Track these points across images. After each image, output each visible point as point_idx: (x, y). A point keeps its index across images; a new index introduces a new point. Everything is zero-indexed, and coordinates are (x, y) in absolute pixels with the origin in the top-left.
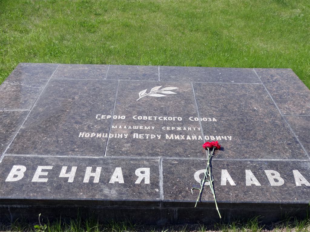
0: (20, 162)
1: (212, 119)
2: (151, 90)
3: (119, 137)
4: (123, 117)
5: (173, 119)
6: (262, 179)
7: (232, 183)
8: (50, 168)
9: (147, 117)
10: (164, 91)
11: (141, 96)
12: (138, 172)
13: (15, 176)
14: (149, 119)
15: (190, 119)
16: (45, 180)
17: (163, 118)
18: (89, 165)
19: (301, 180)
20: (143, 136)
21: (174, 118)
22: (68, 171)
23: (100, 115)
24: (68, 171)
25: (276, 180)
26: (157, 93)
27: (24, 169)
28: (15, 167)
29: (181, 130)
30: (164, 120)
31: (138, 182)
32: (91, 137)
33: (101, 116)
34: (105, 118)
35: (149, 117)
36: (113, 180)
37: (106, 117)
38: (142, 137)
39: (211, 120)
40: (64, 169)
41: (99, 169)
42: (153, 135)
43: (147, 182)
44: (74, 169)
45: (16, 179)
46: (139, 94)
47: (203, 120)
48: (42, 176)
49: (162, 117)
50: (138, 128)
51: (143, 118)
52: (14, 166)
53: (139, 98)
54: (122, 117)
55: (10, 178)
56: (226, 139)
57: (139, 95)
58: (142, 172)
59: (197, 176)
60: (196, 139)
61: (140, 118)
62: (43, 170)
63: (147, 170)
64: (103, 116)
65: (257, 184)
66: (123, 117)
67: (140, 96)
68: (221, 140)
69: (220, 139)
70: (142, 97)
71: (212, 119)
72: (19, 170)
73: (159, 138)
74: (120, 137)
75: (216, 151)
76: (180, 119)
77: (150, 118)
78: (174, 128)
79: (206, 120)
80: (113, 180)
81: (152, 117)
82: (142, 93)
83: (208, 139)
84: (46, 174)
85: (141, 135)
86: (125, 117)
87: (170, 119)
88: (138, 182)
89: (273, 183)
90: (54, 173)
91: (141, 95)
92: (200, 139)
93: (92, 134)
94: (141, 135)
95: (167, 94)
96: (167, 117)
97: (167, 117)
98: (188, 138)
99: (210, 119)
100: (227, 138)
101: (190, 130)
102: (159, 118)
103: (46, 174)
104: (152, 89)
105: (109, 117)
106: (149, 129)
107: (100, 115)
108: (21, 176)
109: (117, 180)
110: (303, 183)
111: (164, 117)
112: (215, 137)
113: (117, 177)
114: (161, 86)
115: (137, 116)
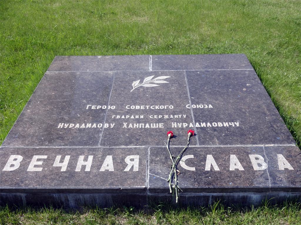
0: (17, 152)
1: (208, 106)
2: (144, 80)
3: (135, 127)
4: (113, 107)
5: (164, 108)
6: (272, 162)
7: (217, 168)
8: (45, 157)
9: (139, 106)
10: (157, 80)
11: (135, 87)
12: (127, 160)
13: (12, 166)
14: (141, 108)
15: (127, 107)
16: (40, 169)
17: (154, 107)
18: (59, 153)
19: (284, 164)
20: (162, 125)
21: (166, 106)
22: (62, 161)
23: (91, 105)
24: (62, 161)
25: (260, 165)
26: (150, 83)
27: (20, 158)
28: (13, 157)
29: (168, 117)
30: (156, 108)
31: (127, 169)
32: (70, 127)
33: (91, 107)
34: (95, 109)
35: (142, 106)
36: (102, 169)
37: (96, 107)
38: (162, 126)
39: (207, 107)
40: (59, 157)
41: (91, 158)
42: (185, 123)
43: (136, 169)
44: (67, 158)
45: (12, 169)
46: (133, 85)
47: (199, 107)
48: (229, 191)
49: (154, 106)
50: (140, 124)
51: (135, 107)
52: (128, 157)
53: (133, 88)
54: (112, 106)
55: (7, 168)
56: (233, 126)
57: (133, 86)
58: (132, 160)
59: (183, 164)
60: (205, 126)
61: (133, 107)
62: (39, 160)
63: (137, 158)
64: (93, 106)
65: (241, 169)
66: (113, 107)
67: (134, 87)
68: (234, 126)
69: (228, 126)
70: (135, 88)
71: (208, 106)
72: (15, 160)
73: (238, 126)
74: (136, 124)
75: (191, 137)
76: (171, 107)
77: (142, 107)
78: (187, 125)
79: (203, 107)
80: (102, 169)
81: (144, 106)
82: (136, 84)
83: (222, 125)
84: (40, 163)
85: (161, 125)
86: (114, 107)
87: (162, 107)
88: (127, 169)
89: (256, 168)
90: (48, 162)
91: (135, 86)
92: (209, 126)
93: (71, 124)
94: (161, 125)
95: (160, 84)
96: (158, 106)
97: (158, 106)
98: (131, 126)
99: (206, 105)
100: (235, 125)
101: (136, 124)
102: (151, 107)
103: (40, 163)
104: (145, 79)
105: (99, 107)
106: (143, 118)
107: (91, 105)
108: (17, 166)
109: (107, 168)
110: (286, 167)
111: (156, 106)
112: (223, 124)
113: (235, 165)
114: (153, 76)
115: (130, 106)
